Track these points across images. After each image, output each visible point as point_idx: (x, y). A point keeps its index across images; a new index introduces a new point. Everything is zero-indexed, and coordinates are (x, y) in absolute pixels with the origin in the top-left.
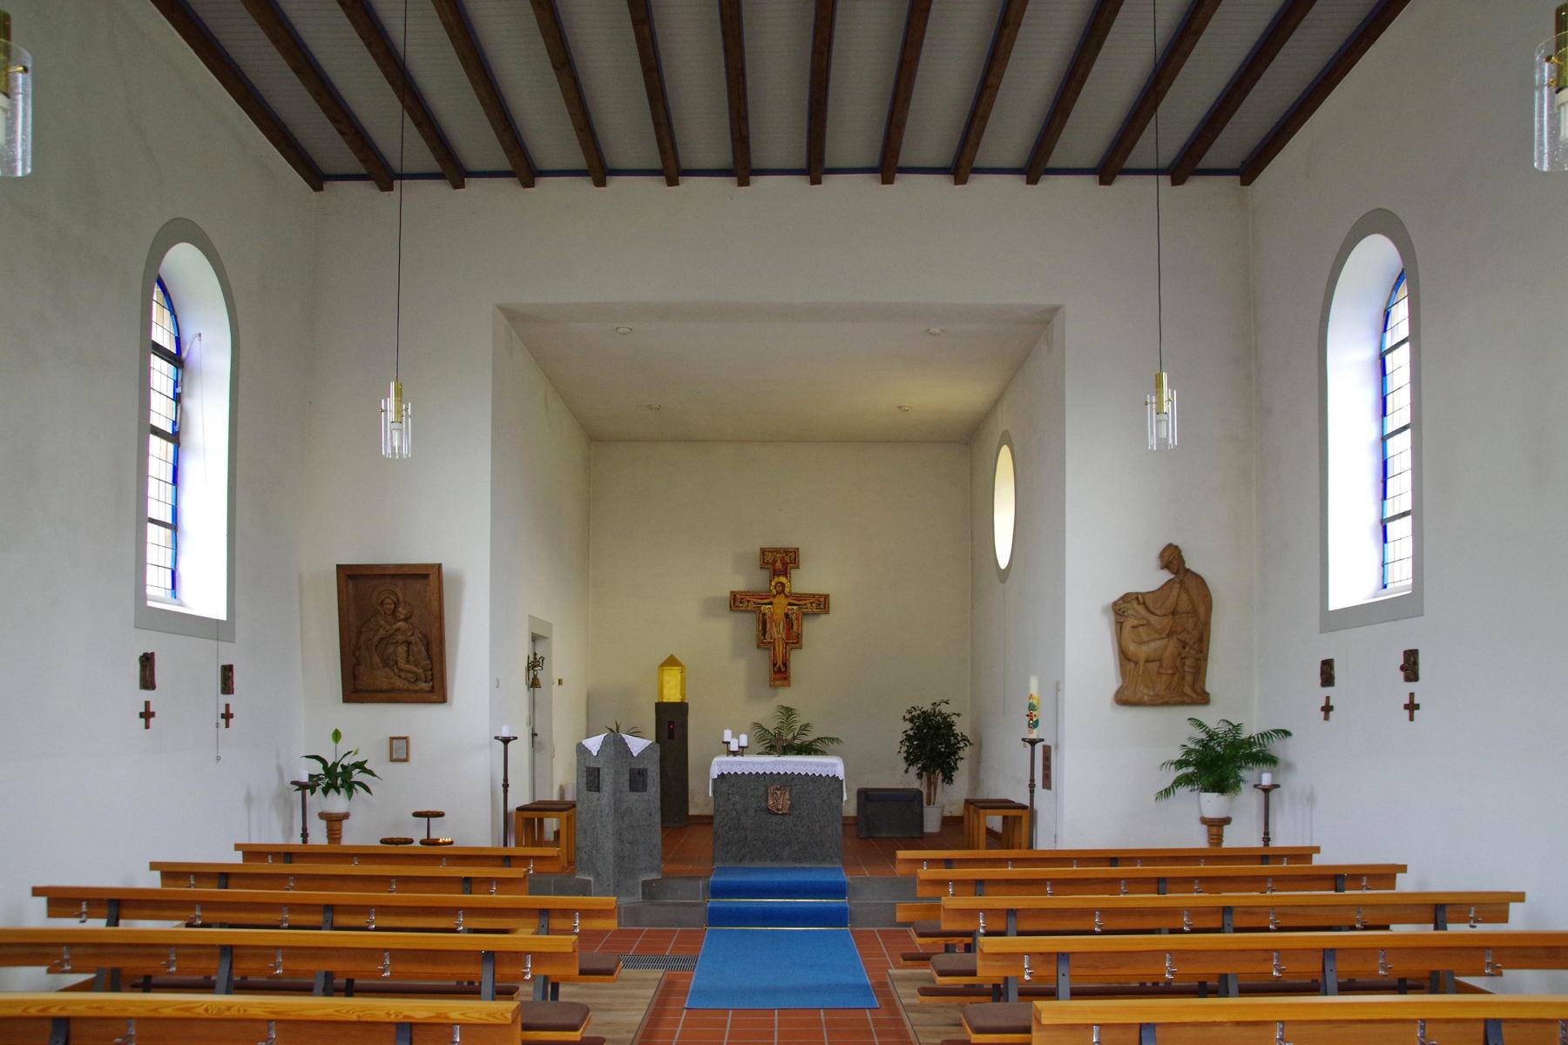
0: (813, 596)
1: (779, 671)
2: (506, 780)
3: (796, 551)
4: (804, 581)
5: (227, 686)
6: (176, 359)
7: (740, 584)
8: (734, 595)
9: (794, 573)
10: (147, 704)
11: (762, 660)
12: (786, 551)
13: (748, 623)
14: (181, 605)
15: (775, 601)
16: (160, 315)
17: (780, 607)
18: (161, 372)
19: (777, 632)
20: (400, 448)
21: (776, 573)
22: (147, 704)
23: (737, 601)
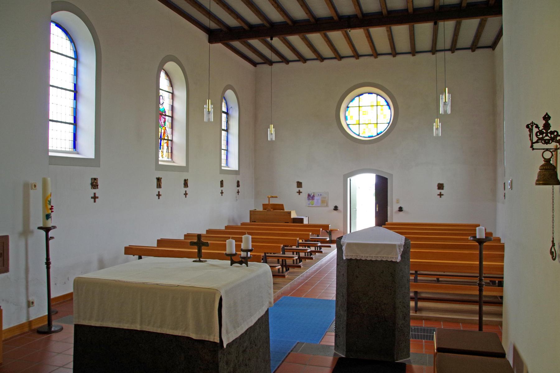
2: (48, 259)
5: (238, 186)
6: (227, 113)
10: (159, 192)
14: (78, 154)
16: (224, 104)
18: (224, 115)
20: (218, 112)
22: (159, 192)
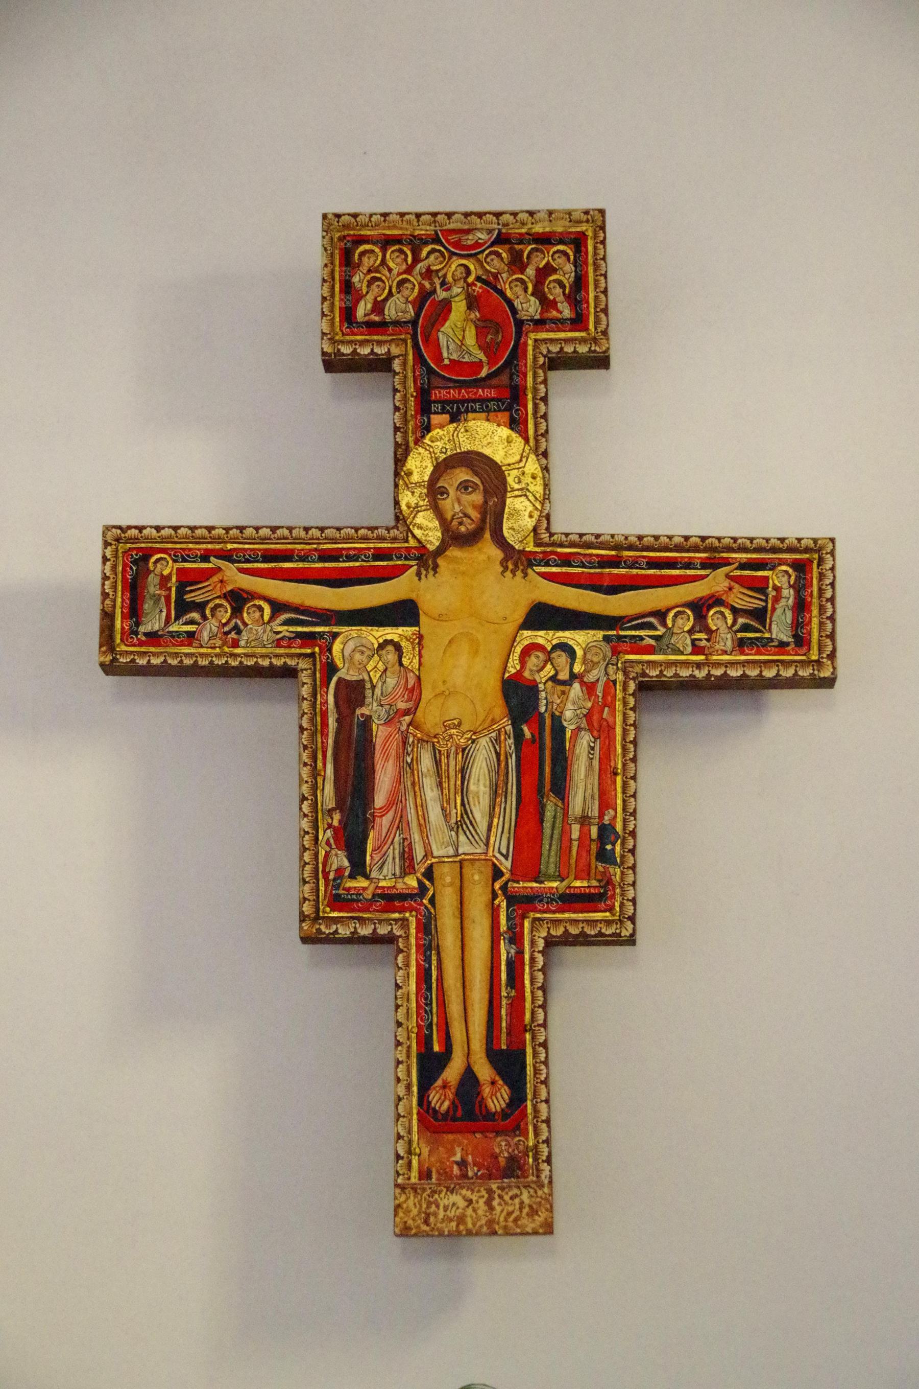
0: (713, 554)
1: (467, 1111)
3: (579, 240)
4: (634, 458)
7: (190, 487)
8: (133, 558)
9: (571, 403)
11: (352, 1018)
12: (516, 240)
13: (243, 759)
15: (434, 592)
17: (467, 636)
19: (450, 820)
21: (437, 395)
23: (162, 604)
